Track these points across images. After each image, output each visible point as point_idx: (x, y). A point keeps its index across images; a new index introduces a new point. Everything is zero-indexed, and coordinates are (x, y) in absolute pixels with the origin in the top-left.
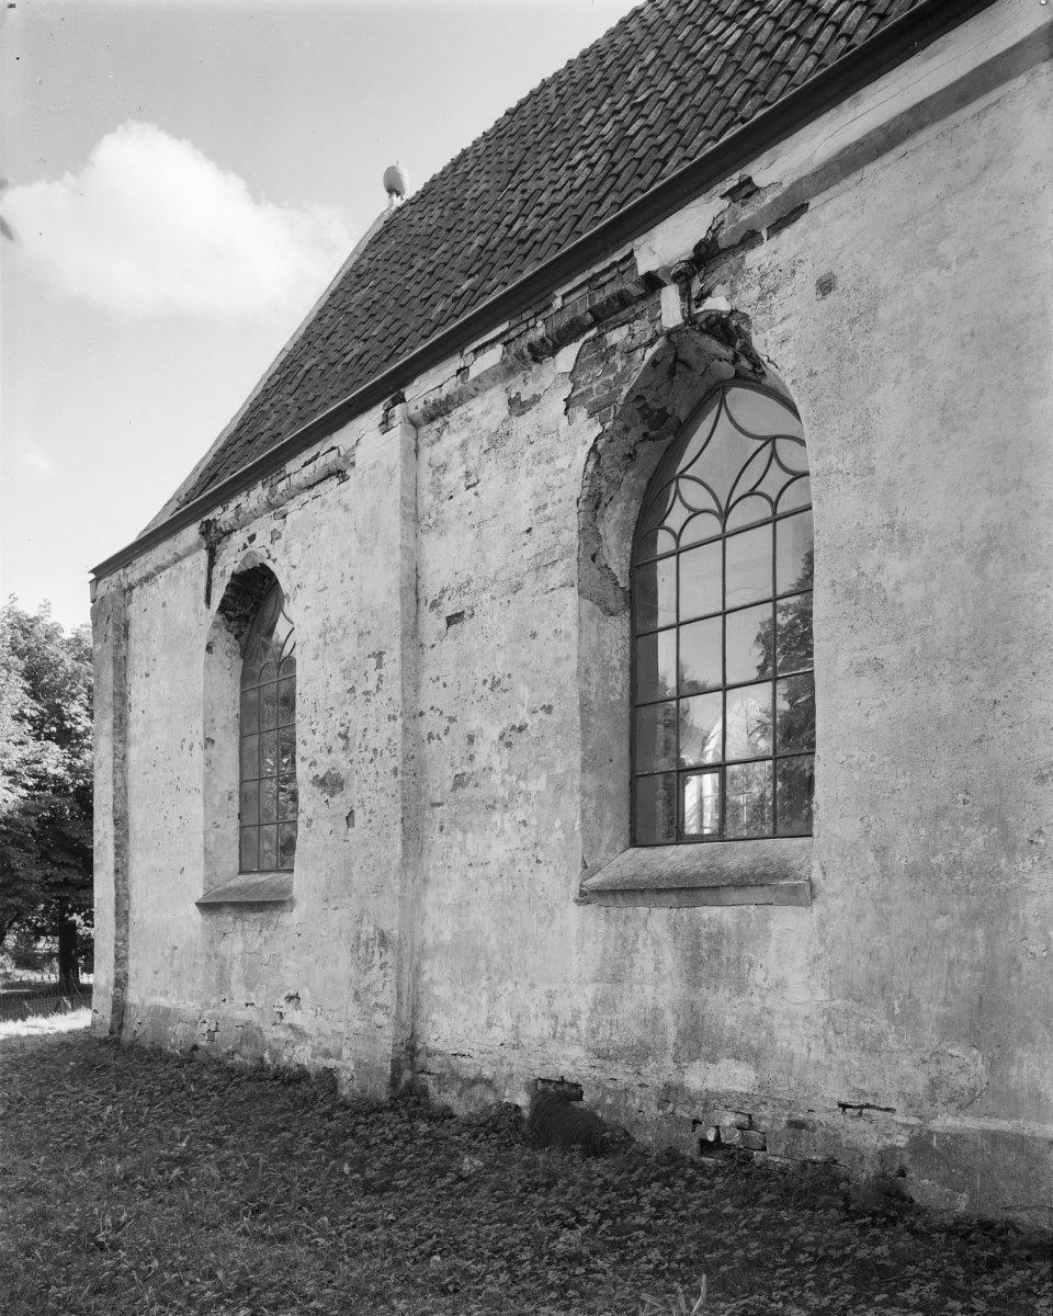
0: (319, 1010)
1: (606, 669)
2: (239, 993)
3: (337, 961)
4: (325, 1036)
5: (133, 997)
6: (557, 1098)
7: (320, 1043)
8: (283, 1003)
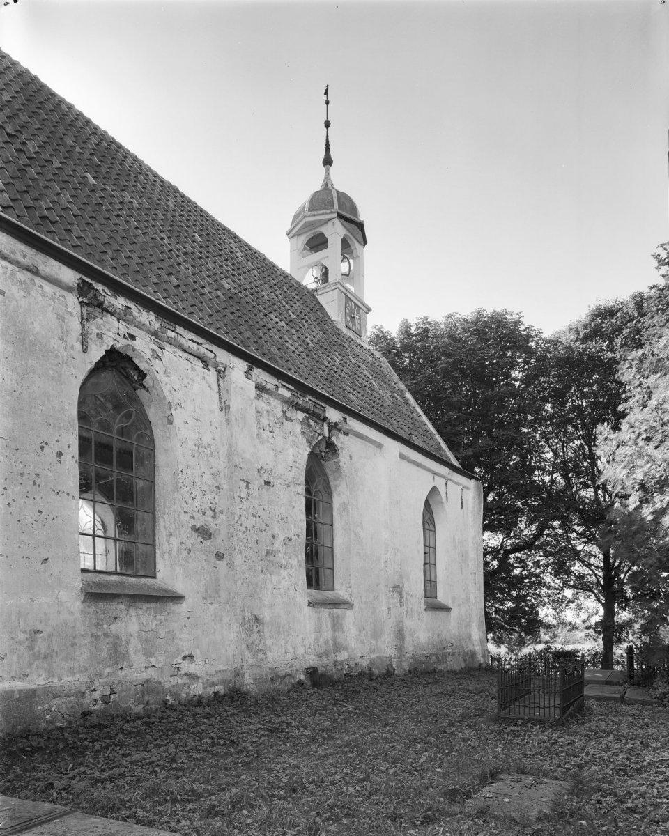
0: (207, 660)
2: (138, 660)
3: (214, 632)
4: (211, 675)
6: (312, 672)
7: (207, 680)
8: (180, 660)
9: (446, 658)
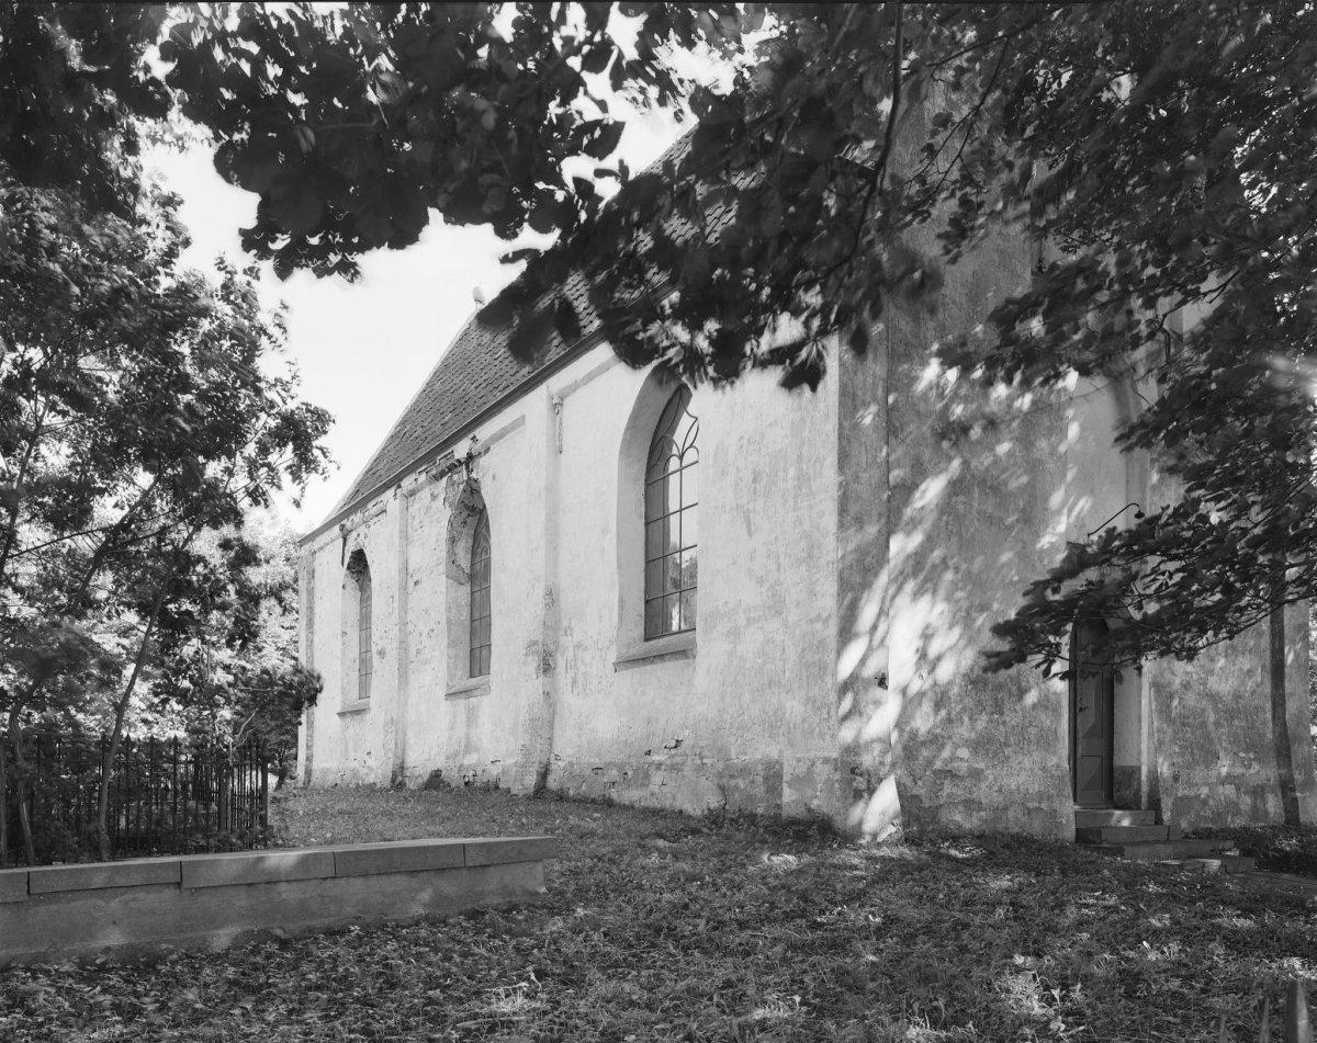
1: (459, 606)
2: (352, 755)
5: (315, 766)
9: (647, 776)
